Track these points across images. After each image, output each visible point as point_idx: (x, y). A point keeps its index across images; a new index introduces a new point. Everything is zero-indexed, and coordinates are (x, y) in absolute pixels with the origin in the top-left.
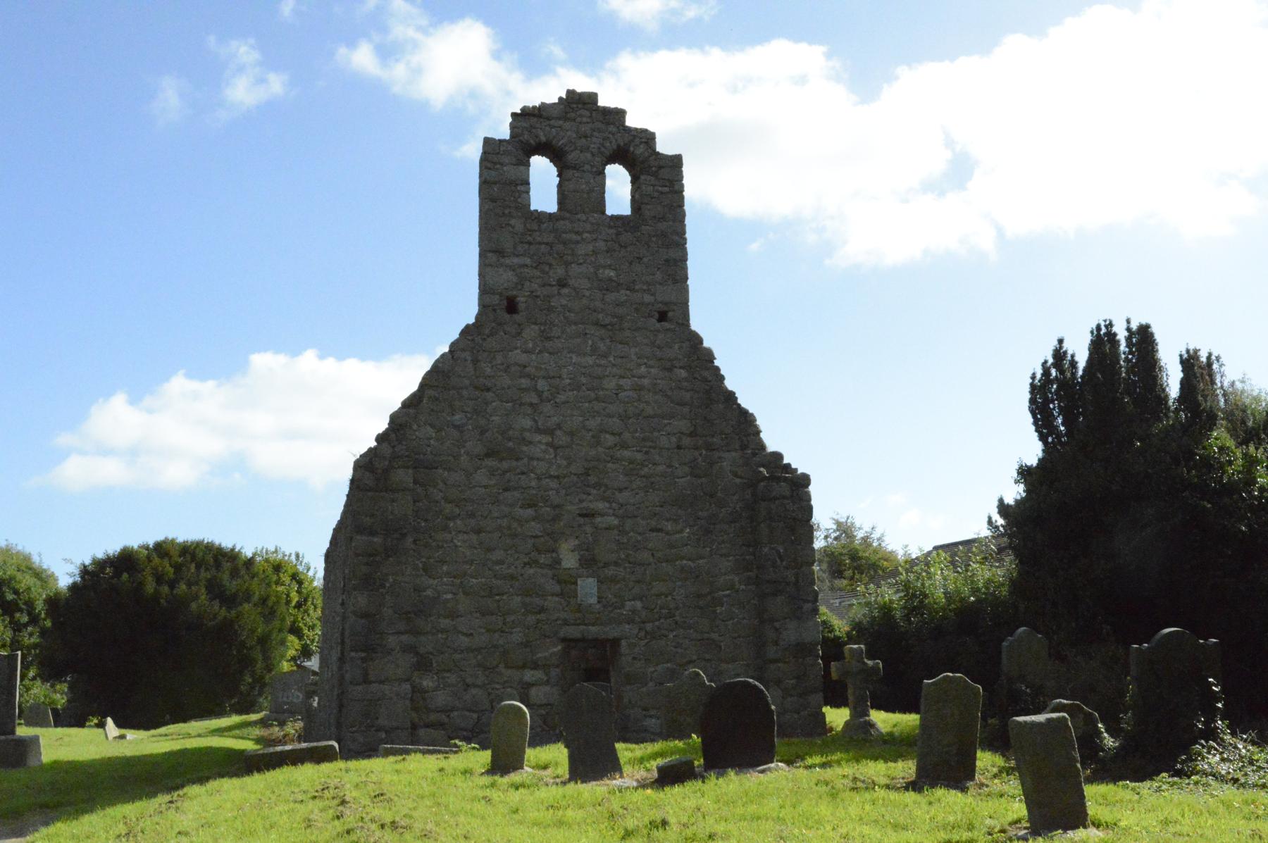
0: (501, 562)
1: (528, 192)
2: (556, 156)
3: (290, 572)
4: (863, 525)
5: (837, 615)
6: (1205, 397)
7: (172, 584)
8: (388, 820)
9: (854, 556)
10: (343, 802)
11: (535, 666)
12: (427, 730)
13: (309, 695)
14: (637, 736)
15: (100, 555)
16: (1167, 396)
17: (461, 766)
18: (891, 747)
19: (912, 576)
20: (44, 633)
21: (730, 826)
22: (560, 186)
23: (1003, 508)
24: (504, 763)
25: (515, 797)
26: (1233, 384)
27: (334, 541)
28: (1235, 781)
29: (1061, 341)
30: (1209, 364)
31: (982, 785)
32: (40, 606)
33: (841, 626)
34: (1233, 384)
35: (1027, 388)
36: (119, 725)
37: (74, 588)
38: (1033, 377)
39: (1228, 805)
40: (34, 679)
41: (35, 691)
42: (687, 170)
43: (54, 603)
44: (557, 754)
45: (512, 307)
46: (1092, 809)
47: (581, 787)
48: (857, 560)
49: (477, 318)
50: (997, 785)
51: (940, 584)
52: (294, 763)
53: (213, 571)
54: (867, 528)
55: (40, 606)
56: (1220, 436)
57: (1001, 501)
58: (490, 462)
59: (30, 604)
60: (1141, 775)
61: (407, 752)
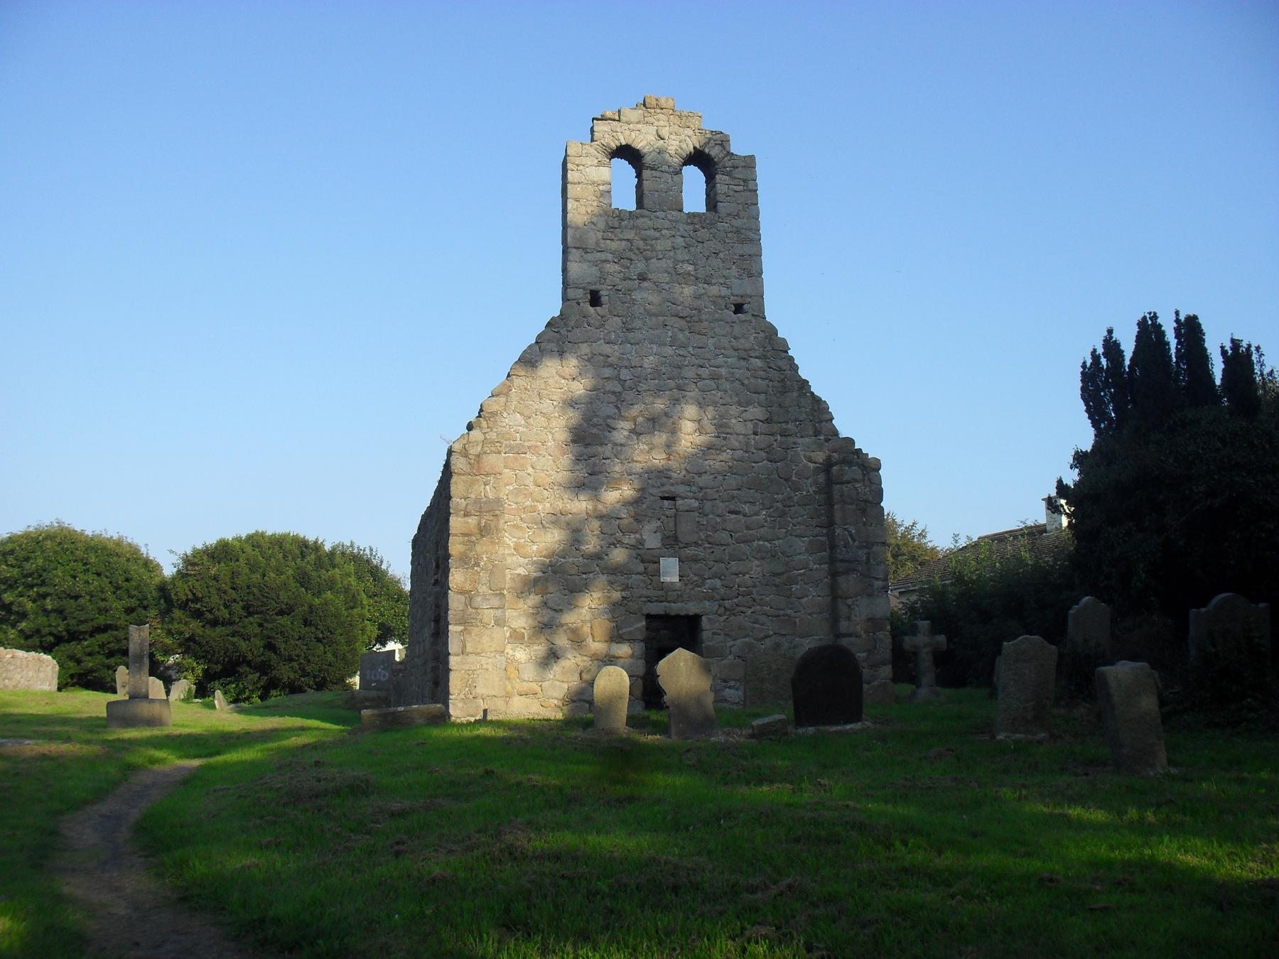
15: (200, 546)
29: (1110, 332)
35: (1079, 377)
45: (595, 300)
54: (908, 523)
57: (1060, 482)
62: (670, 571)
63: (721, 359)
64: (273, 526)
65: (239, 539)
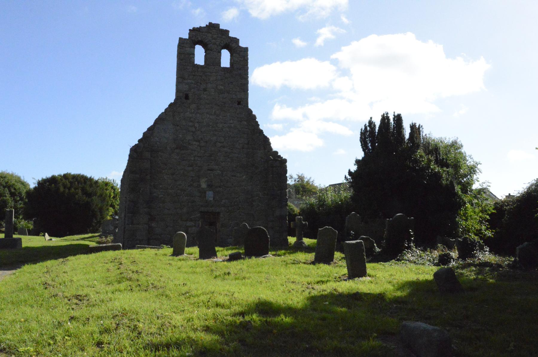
0: (180, 185)
1: (194, 57)
2: (205, 46)
3: (111, 186)
4: (307, 176)
5: (295, 206)
6: (416, 139)
7: (69, 189)
8: (135, 270)
9: (303, 187)
10: (121, 264)
11: (191, 220)
12: (153, 241)
13: (116, 227)
14: (224, 245)
15: (44, 178)
16: (405, 138)
17: (163, 253)
18: (308, 249)
19: (321, 194)
20: (25, 203)
21: (251, 275)
22: (205, 56)
23: (350, 173)
24: (178, 252)
25: (180, 263)
26: (426, 135)
27: (124, 176)
28: (415, 262)
29: (371, 118)
30: (419, 128)
31: (336, 263)
32: (24, 194)
33: (297, 210)
34: (426, 135)
35: (359, 133)
36: (50, 235)
37: (35, 188)
38: (362, 130)
39: (411, 270)
40: (22, 219)
41: (22, 223)
42: (250, 53)
43: (29, 193)
44: (196, 250)
45: (187, 97)
46: (369, 271)
47: (202, 261)
48: (304, 188)
49: (175, 100)
50: (340, 263)
51: (330, 197)
52: (106, 250)
53: (83, 185)
54: (308, 178)
55: (24, 194)
56: (420, 152)
57: (349, 170)
58: (178, 151)
59: (20, 193)
60: (385, 261)
61: (145, 248)
62: (210, 195)
63: (231, 121)
64: (74, 171)
65: (60, 176)
